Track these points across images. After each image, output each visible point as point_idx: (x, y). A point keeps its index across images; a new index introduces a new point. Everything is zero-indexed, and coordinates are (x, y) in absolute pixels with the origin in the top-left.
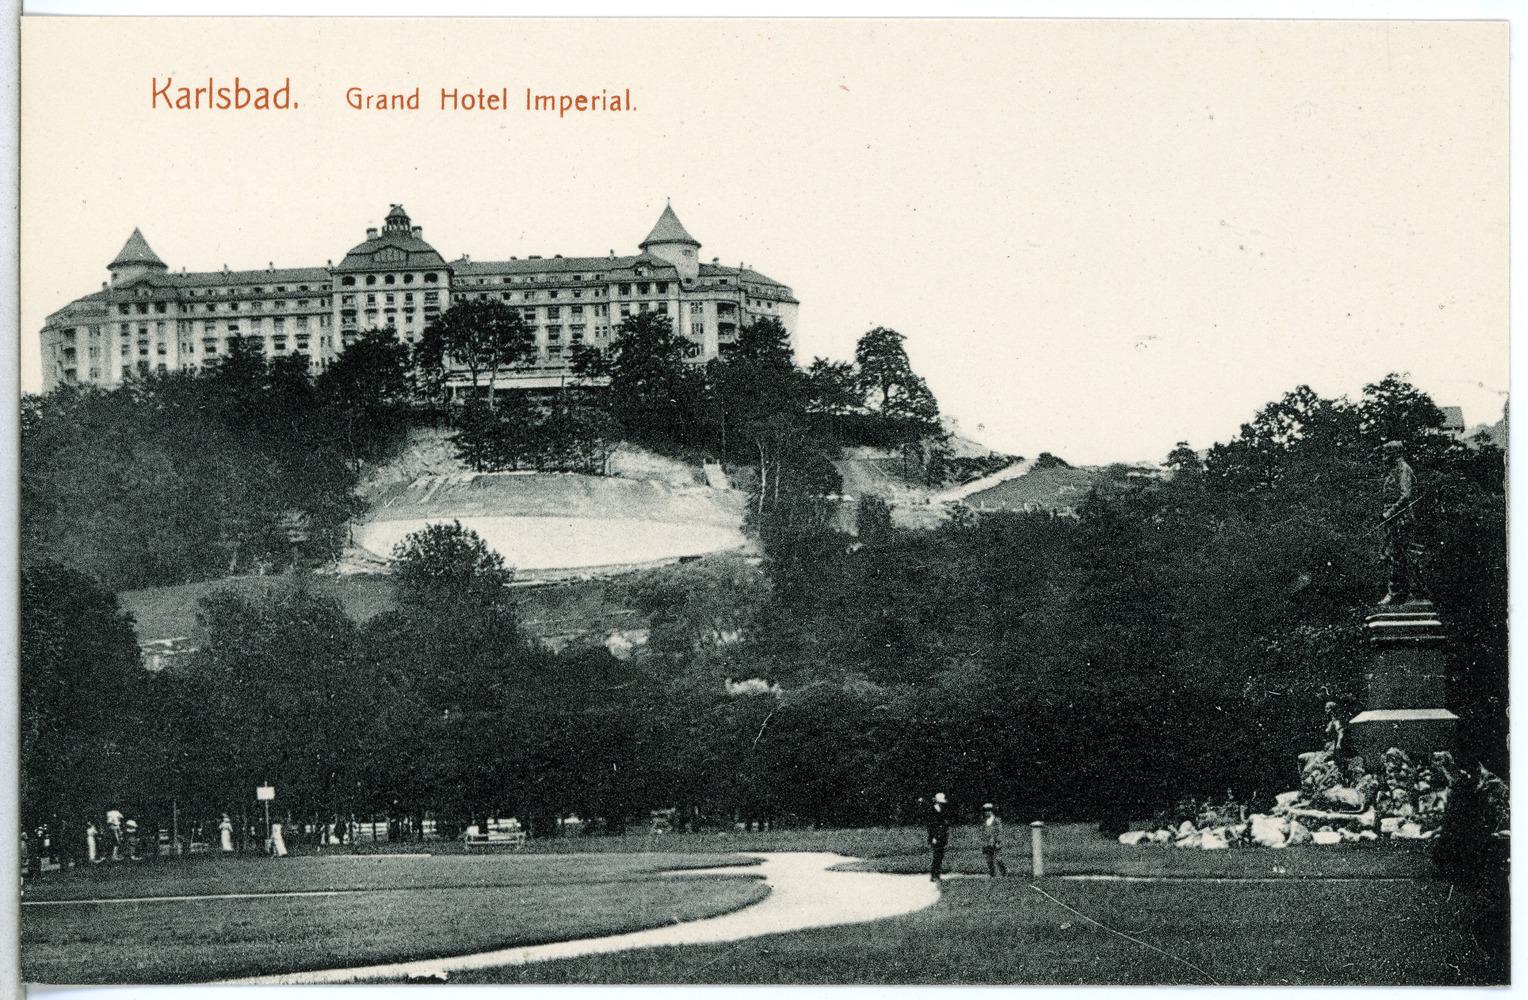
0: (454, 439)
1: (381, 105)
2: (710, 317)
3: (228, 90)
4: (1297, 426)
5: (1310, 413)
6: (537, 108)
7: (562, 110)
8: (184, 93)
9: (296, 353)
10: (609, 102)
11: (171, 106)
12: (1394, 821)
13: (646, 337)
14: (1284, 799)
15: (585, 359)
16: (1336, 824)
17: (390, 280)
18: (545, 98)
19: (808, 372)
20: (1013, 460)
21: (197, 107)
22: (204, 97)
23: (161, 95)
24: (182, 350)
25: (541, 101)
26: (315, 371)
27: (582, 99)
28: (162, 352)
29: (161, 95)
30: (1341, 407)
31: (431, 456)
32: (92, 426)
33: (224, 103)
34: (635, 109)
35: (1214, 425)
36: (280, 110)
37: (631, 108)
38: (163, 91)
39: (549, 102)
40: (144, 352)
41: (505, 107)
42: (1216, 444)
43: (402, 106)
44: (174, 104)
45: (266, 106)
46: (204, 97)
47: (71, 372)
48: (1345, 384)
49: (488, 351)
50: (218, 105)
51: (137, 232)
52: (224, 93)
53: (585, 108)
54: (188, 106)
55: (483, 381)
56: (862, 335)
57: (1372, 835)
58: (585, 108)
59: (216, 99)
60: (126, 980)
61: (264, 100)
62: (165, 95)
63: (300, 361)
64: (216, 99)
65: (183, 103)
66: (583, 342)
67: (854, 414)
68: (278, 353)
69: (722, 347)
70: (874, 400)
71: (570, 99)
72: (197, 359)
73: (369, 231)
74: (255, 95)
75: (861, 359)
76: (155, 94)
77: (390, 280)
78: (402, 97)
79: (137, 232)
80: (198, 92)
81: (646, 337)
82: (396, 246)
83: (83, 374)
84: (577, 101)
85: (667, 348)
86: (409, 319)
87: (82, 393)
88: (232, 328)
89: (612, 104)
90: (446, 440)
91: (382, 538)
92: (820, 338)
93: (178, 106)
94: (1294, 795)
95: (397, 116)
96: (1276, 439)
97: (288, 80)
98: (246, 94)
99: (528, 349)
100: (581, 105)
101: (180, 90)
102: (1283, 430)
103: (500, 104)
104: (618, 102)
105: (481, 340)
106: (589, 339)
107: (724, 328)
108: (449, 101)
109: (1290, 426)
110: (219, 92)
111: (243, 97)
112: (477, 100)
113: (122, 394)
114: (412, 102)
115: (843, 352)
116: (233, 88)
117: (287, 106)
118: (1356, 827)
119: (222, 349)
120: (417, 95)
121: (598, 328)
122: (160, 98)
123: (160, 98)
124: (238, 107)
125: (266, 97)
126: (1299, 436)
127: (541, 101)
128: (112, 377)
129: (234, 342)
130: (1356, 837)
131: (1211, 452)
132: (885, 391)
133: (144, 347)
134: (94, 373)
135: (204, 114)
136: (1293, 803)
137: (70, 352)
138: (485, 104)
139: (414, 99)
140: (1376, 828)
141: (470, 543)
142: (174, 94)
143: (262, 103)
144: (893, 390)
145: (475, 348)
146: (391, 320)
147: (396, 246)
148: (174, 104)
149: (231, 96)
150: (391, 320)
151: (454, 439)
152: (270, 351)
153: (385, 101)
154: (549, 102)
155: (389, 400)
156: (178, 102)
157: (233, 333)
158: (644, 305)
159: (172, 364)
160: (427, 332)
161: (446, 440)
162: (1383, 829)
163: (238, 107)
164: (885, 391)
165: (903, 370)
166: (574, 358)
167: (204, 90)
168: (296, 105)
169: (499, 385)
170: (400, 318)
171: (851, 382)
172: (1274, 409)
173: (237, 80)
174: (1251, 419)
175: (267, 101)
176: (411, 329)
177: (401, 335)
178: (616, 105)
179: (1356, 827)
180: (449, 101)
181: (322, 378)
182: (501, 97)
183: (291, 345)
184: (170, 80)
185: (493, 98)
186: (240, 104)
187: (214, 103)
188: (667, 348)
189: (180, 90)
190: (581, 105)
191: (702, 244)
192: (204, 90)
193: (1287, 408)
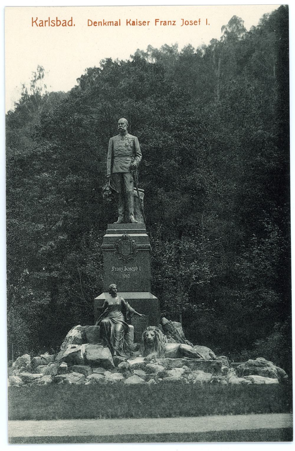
1: (165, 24)
3: (54, 21)
8: (41, 22)
11: (37, 26)
18: (110, 22)
22: (47, 23)
23: (35, 23)
25: (109, 23)
27: (144, 22)
29: (35, 23)
32: (68, 149)
33: (53, 25)
36: (186, 25)
38: (129, 22)
39: (112, 23)
44: (38, 25)
46: (47, 23)
50: (51, 25)
51: (283, 13)
52: (53, 22)
53: (197, 24)
54: (42, 26)
58: (197, 24)
59: (51, 23)
60: (247, 440)
61: (65, 24)
62: (36, 23)
64: (51, 23)
65: (41, 25)
74: (62, 22)
76: (33, 22)
79: (283, 13)
80: (45, 21)
84: (94, 23)
98: (91, 22)
100: (95, 24)
101: (40, 21)
104: (117, 23)
110: (139, 22)
111: (59, 23)
114: (186, 23)
116: (56, 21)
117: (72, 25)
120: (72, 20)
122: (34, 23)
123: (34, 23)
124: (57, 26)
125: (66, 23)
127: (109, 23)
135: (47, 28)
139: (71, 22)
142: (131, 23)
143: (64, 24)
148: (38, 25)
149: (55, 22)
154: (112, 23)
156: (39, 24)
163: (57, 26)
167: (47, 21)
168: (74, 25)
173: (57, 18)
175: (66, 24)
178: (116, 24)
184: (37, 18)
185: (196, 22)
189: (40, 21)
190: (95, 24)
191: (284, 3)
192: (47, 21)
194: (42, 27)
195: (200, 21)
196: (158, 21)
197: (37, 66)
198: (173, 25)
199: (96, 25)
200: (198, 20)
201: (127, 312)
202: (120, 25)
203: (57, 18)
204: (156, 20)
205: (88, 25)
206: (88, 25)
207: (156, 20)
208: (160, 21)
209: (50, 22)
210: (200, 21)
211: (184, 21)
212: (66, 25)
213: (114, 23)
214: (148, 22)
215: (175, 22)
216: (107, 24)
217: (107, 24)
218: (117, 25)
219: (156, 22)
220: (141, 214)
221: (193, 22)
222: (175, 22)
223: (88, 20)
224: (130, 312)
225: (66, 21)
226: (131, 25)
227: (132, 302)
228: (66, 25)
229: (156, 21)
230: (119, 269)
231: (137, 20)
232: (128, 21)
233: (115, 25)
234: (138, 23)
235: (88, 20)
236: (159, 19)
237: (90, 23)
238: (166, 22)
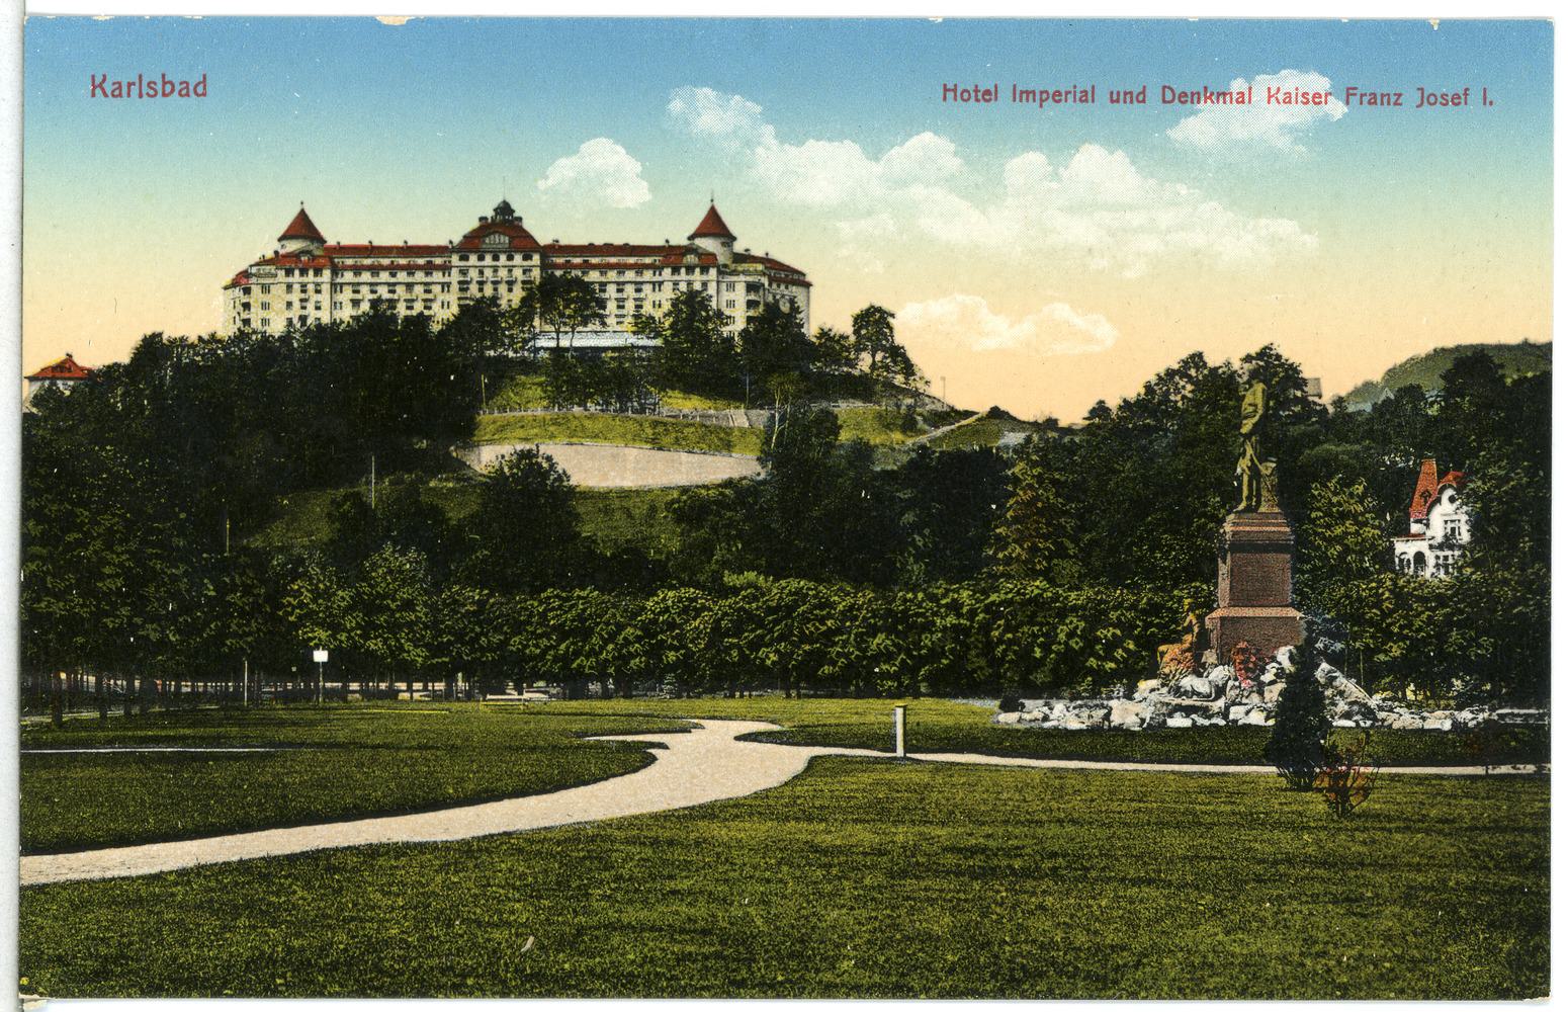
0: (540, 384)
2: (740, 295)
4: (1189, 387)
5: (1200, 378)
7: (1042, 101)
9: (421, 313)
10: (1078, 95)
12: (1242, 709)
13: (692, 308)
14: (1144, 686)
15: (644, 325)
16: (1188, 711)
17: (495, 258)
18: (1028, 93)
19: (814, 340)
20: (967, 414)
22: (135, 90)
24: (337, 306)
25: (1024, 96)
26: (436, 328)
28: (318, 308)
30: (1224, 373)
31: (531, 403)
33: (152, 92)
35: (1123, 386)
38: (100, 86)
39: (1031, 96)
40: (304, 308)
42: (1125, 401)
46: (135, 90)
47: (246, 322)
48: (1227, 351)
49: (569, 317)
50: (148, 94)
54: (120, 95)
55: (565, 343)
56: (857, 311)
57: (1222, 723)
59: (145, 90)
61: (1028, 94)
63: (422, 321)
65: (117, 93)
66: (643, 311)
67: (849, 374)
68: (409, 313)
69: (749, 320)
70: (865, 361)
71: (1435, 96)
72: (346, 314)
73: (481, 219)
74: (178, 88)
75: (856, 332)
76: (94, 88)
77: (495, 258)
78: (1034, 92)
81: (692, 308)
82: (502, 229)
83: (256, 324)
84: (1180, 96)
85: (708, 319)
86: (510, 290)
87: (254, 337)
88: (373, 292)
90: (534, 384)
91: (487, 458)
92: (828, 313)
93: (113, 96)
94: (1153, 683)
96: (1172, 398)
99: (602, 318)
100: (1456, 101)
102: (1177, 391)
104: (1290, 97)
105: (565, 308)
106: (647, 309)
107: (750, 304)
108: (950, 95)
109: (1184, 387)
110: (149, 84)
112: (973, 94)
113: (286, 339)
115: (843, 326)
118: (1205, 712)
119: (365, 307)
121: (659, 300)
122: (98, 91)
123: (98, 91)
125: (187, 88)
126: (1190, 395)
127: (1024, 96)
128: (277, 328)
129: (375, 303)
130: (1206, 722)
131: (1120, 408)
132: (873, 356)
133: (304, 304)
134: (265, 322)
136: (1153, 690)
137: (247, 306)
138: (980, 97)
140: (1225, 714)
141: (545, 465)
143: (184, 92)
144: (879, 356)
145: (562, 315)
146: (496, 289)
147: (502, 229)
149: (159, 87)
150: (496, 289)
151: (540, 384)
152: (402, 310)
153: (120, 88)
154: (1031, 96)
155: (492, 353)
157: (375, 296)
158: (689, 283)
159: (326, 320)
160: (523, 300)
161: (534, 384)
162: (1231, 717)
164: (873, 356)
165: (888, 341)
166: (636, 324)
167: (134, 84)
169: (577, 343)
170: (503, 289)
171: (848, 350)
172: (1171, 373)
173: (163, 76)
174: (1153, 379)
176: (511, 298)
177: (503, 303)
179: (1205, 712)
180: (950, 95)
181: (441, 332)
182: (993, 90)
183: (418, 307)
185: (988, 92)
188: (708, 319)
190: (987, 97)
193: (1182, 372)
194: (1374, 106)
195: (1466, 94)
196: (1355, 94)
197: (700, 215)
198: (1396, 104)
199: (1459, 103)
200: (971, 89)
202: (1093, 101)
203: (163, 76)
205: (1164, 101)
206: (1164, 101)
207: (1348, 89)
208: (1358, 92)
209: (144, 84)
210: (1466, 94)
211: (1426, 95)
212: (188, 95)
213: (1235, 96)
215: (1400, 95)
218: (1290, 102)
219: (1348, 95)
220: (1495, 884)
221: (1310, 97)
222: (1400, 95)
223: (1164, 87)
225: (188, 84)
226: (106, 96)
228: (188, 95)
231: (1297, 89)
232: (97, 82)
233: (1238, 102)
234: (1300, 98)
235: (1164, 87)
236: (1355, 88)
237: (1169, 96)
238: (1375, 94)
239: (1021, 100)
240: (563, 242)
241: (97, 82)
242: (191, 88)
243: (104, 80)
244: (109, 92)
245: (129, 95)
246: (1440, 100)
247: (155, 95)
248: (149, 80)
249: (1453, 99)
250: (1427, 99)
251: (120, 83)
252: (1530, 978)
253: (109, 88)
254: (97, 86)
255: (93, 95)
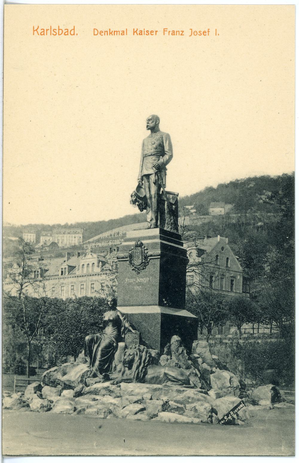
6: (117, 35)
8: (43, 30)
11: (39, 35)
18: (117, 32)
21: (127, 34)
22: (49, 32)
34: (77, 34)
37: (217, 34)
38: (36, 30)
39: (118, 32)
41: (208, 35)
43: (107, 35)
45: (68, 34)
46: (49, 32)
50: (146, 34)
52: (55, 31)
54: (44, 34)
59: (52, 32)
61: (67, 32)
64: (52, 32)
65: (141, 34)
71: (196, 32)
74: (64, 31)
76: (34, 31)
80: (47, 30)
89: (122, 33)
93: (41, 35)
95: (177, 37)
97: (74, 26)
100: (205, 34)
101: (41, 29)
103: (207, 34)
110: (53, 30)
111: (60, 31)
114: (193, 33)
116: (57, 29)
117: (74, 34)
120: (74, 29)
122: (135, 33)
123: (135, 33)
124: (59, 35)
125: (68, 31)
127: (116, 33)
135: (48, 37)
142: (39, 31)
143: (66, 33)
148: (40, 34)
149: (57, 31)
154: (118, 32)
156: (41, 33)
163: (59, 35)
167: (49, 30)
182: (50, 29)
184: (38, 27)
186: (60, 34)
187: (145, 34)
189: (41, 29)
190: (205, 34)
192: (49, 30)
195: (208, 31)
196: (167, 31)
198: (181, 35)
201: (123, 328)
204: (164, 29)
205: (94, 35)
206: (94, 35)
210: (208, 31)
213: (121, 32)
214: (156, 31)
215: (183, 32)
216: (113, 33)
217: (113, 33)
219: (164, 31)
222: (183, 32)
223: (94, 29)
224: (126, 328)
225: (68, 30)
227: (127, 316)
229: (165, 30)
230: (132, 281)
231: (144, 29)
232: (135, 31)
234: (146, 33)
235: (94, 29)
239: (114, 35)
240: (69, 224)
241: (135, 31)
242: (69, 31)
243: (137, 31)
244: (39, 33)
245: (176, 35)
246: (198, 33)
247: (149, 34)
248: (147, 30)
249: (203, 33)
250: (193, 33)
251: (124, 31)
252: (294, 6)
253: (138, 32)
254: (35, 30)
255: (134, 34)
